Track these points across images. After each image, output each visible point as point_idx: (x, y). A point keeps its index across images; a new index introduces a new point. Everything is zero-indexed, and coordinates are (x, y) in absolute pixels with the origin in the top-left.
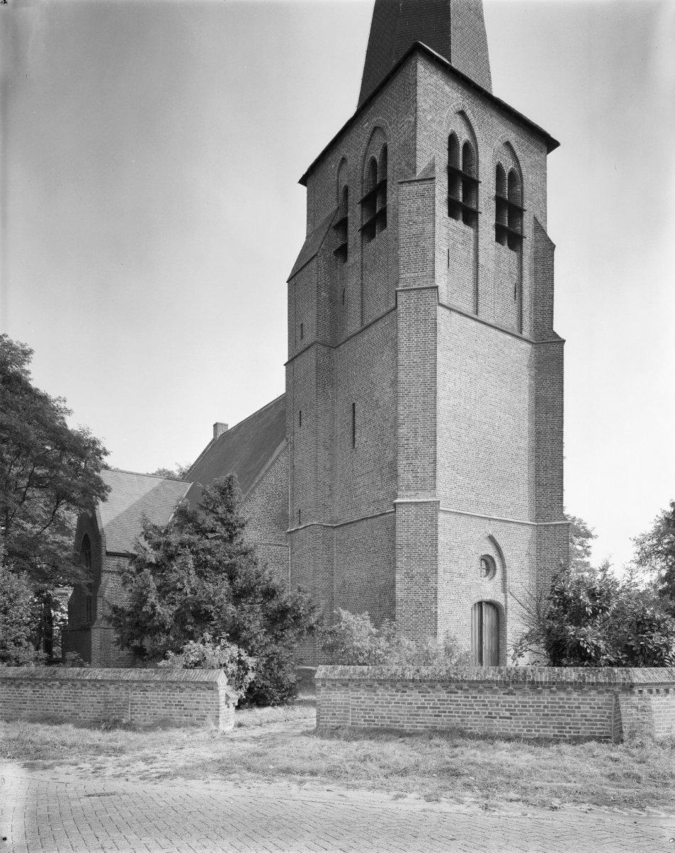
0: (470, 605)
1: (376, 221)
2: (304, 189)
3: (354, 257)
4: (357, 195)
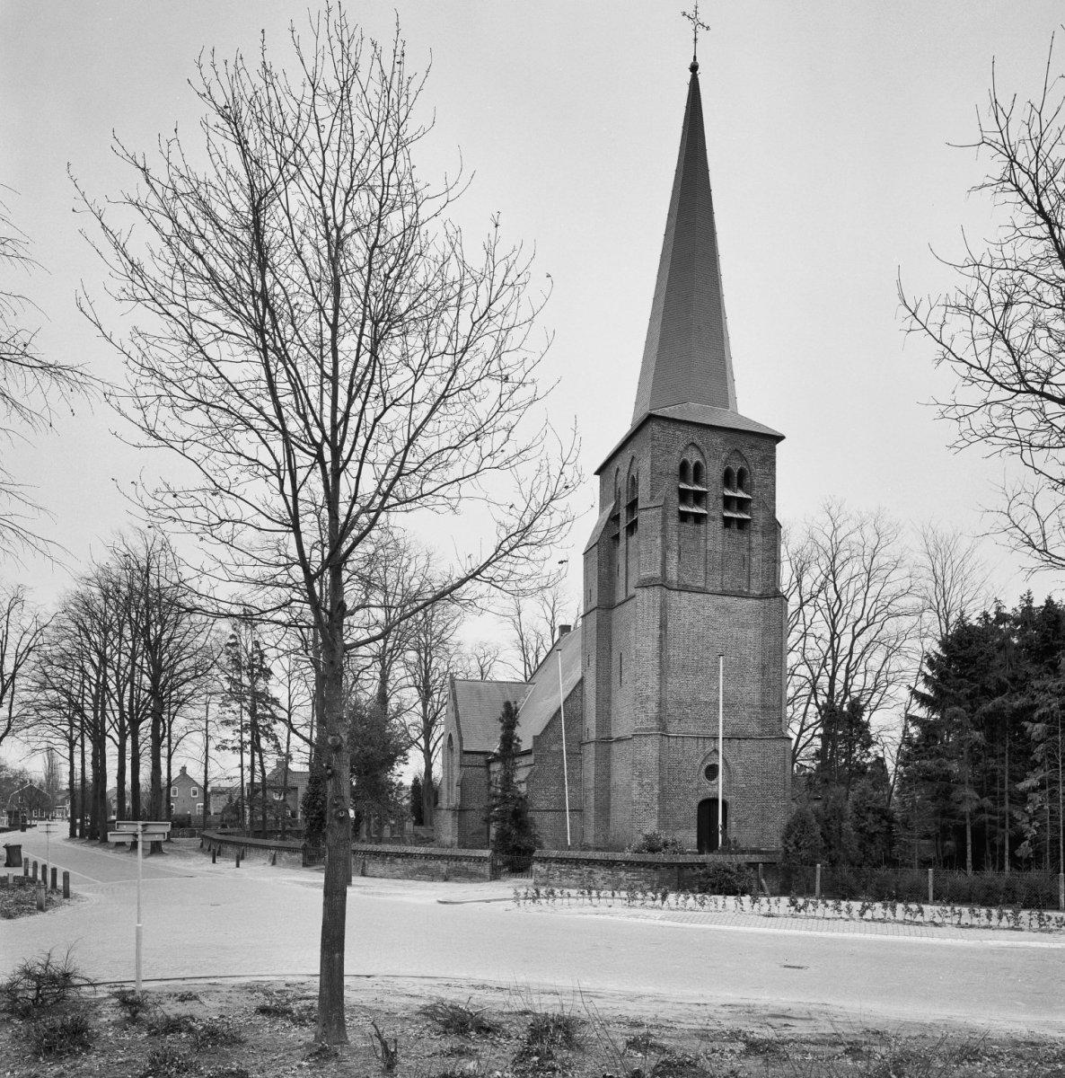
0: (695, 804)
1: (632, 528)
2: (598, 477)
3: (622, 544)
4: (624, 502)
